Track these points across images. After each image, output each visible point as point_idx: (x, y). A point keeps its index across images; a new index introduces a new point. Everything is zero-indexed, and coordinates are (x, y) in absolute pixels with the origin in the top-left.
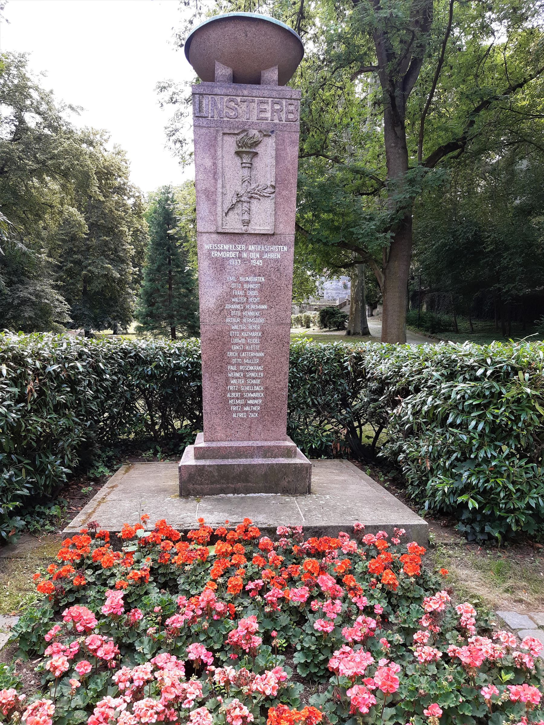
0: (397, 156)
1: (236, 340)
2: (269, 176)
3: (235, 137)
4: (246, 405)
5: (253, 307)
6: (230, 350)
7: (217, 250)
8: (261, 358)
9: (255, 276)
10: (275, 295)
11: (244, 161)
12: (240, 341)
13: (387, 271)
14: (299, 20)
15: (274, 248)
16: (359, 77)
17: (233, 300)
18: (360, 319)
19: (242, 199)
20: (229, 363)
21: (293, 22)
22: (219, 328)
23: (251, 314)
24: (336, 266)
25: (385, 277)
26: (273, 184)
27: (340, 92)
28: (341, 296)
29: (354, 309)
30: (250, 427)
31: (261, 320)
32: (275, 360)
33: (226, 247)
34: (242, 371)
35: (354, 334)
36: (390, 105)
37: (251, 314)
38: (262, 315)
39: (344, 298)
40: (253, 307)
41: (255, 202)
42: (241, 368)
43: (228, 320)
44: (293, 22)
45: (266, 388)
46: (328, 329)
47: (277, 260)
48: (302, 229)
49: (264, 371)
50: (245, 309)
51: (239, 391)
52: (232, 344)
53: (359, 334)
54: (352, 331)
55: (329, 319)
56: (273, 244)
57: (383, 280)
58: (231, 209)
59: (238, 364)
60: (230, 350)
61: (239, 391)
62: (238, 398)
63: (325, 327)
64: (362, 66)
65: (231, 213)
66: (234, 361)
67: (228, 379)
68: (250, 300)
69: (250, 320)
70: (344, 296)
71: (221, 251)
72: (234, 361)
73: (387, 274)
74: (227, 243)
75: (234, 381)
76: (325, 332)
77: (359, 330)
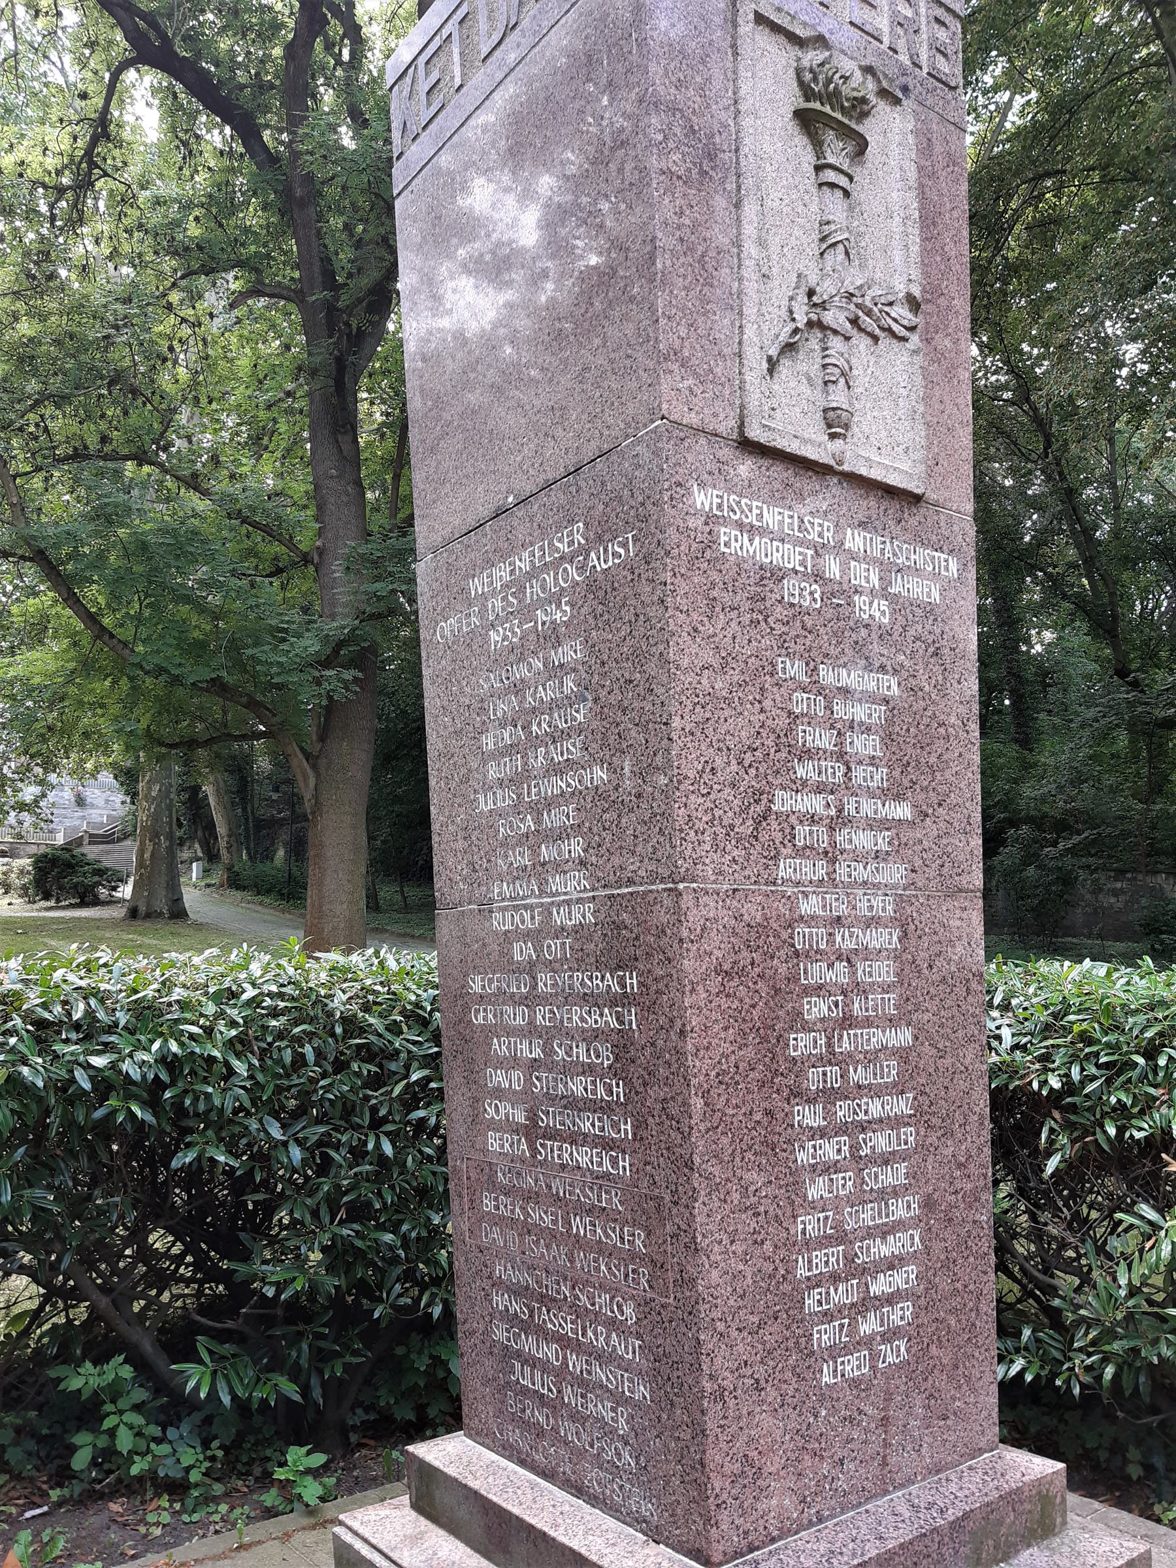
0: (345, 499)
1: (817, 972)
2: (898, 256)
3: (795, 51)
4: (866, 1304)
5: (868, 807)
6: (797, 1021)
7: (740, 525)
8: (902, 1055)
9: (869, 668)
10: (933, 759)
11: (831, 160)
12: (830, 976)
13: (323, 762)
14: (94, 142)
15: (921, 556)
16: (250, 302)
17: (801, 772)
18: (163, 880)
19: (829, 317)
20: (797, 1094)
21: (75, 138)
22: (752, 912)
23: (863, 840)
24: (161, 744)
25: (318, 776)
26: (916, 291)
27: (186, 331)
28: (68, 823)
29: (147, 855)
30: (885, 1422)
31: (894, 873)
32: (948, 1061)
33: (772, 517)
34: (843, 1129)
35: (148, 916)
36: (331, 382)
37: (863, 840)
38: (899, 848)
39: (76, 829)
40: (868, 807)
41: (862, 347)
42: (842, 1110)
43: (784, 869)
44: (75, 138)
45: (928, 1204)
46: (52, 903)
47: (929, 611)
48: (112, 636)
49: (919, 1116)
50: (840, 820)
51: (841, 1237)
52: (807, 991)
53: (160, 915)
54: (143, 909)
55: (61, 876)
56: (920, 540)
57: (312, 781)
58: (789, 348)
59: (829, 1096)
60: (797, 1021)
61: (841, 1237)
62: (835, 1278)
63: (46, 897)
64: (260, 281)
65: (785, 368)
66: (813, 1079)
67: (794, 1180)
68: (859, 773)
69: (861, 872)
70: (77, 823)
71: (752, 530)
72: (813, 1079)
73: (322, 771)
74: (775, 498)
75: (816, 1190)
76: (39, 910)
77: (162, 905)
